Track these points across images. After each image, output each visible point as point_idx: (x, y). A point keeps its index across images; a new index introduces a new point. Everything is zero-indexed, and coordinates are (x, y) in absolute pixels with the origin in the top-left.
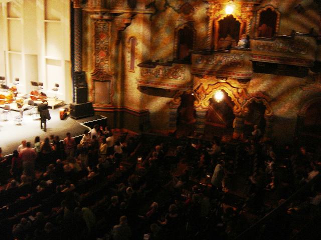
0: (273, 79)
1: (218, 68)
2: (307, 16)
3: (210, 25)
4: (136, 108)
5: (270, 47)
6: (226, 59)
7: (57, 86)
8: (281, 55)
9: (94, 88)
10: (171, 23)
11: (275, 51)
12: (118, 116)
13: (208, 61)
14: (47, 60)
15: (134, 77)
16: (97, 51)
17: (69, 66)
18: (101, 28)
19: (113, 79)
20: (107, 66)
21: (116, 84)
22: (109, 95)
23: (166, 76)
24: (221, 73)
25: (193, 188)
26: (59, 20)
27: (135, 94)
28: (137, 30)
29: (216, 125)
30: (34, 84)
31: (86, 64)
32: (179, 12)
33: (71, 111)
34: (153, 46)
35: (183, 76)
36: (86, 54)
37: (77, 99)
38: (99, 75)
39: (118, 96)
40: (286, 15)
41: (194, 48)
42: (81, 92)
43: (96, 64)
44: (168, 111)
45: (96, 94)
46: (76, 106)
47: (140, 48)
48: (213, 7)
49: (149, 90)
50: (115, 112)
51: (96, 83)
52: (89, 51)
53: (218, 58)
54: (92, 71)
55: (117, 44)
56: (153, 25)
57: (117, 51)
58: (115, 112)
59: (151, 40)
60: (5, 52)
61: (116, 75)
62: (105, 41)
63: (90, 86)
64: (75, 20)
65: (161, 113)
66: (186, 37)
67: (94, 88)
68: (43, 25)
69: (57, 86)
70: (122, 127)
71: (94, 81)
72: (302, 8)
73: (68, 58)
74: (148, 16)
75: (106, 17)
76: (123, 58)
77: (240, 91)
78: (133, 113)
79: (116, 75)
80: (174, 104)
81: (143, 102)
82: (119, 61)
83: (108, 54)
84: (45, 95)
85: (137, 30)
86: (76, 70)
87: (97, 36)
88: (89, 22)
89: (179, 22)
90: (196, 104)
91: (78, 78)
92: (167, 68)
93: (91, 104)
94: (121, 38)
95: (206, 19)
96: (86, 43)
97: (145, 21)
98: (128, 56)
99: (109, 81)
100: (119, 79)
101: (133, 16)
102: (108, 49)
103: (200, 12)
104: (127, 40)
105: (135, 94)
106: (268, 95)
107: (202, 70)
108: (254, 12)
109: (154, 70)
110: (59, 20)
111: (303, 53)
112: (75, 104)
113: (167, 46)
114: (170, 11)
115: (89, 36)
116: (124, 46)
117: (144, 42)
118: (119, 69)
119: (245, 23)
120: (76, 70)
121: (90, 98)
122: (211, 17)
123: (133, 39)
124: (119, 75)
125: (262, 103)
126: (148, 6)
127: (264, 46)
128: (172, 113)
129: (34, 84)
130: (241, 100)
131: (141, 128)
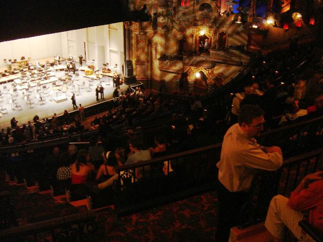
0: (225, 67)
1: (195, 63)
2: (241, 36)
3: (194, 38)
4: (158, 79)
5: (218, 55)
6: (199, 59)
7: (116, 65)
8: (224, 58)
9: (136, 68)
10: (175, 36)
11: (221, 56)
12: (149, 82)
13: (190, 60)
14: (110, 50)
15: (156, 63)
16: (138, 49)
17: (123, 56)
18: (139, 38)
19: (146, 64)
20: (143, 57)
21: (148, 66)
22: (144, 72)
23: (171, 66)
24: (198, 65)
25: (284, 119)
26: (117, 30)
27: (157, 72)
28: (158, 39)
29: (203, 88)
30: (105, 65)
31: (132, 56)
32: (178, 31)
33: (125, 81)
34: (166, 47)
35: (179, 66)
36: (132, 51)
37: (128, 74)
38: (139, 62)
39: (149, 72)
40: (231, 35)
41: (186, 51)
42: (130, 72)
43: (137, 56)
44: (174, 81)
45: (137, 72)
46: (128, 78)
47: (160, 49)
48: (196, 30)
49: (165, 72)
50: (148, 81)
51: (137, 66)
52: (133, 49)
53: (195, 58)
54: (135, 60)
55: (148, 46)
56: (166, 36)
57: (148, 49)
58: (148, 81)
59: (165, 45)
60: (85, 43)
61: (148, 61)
62: (142, 44)
63: (134, 67)
64: (126, 35)
65: (171, 81)
66: (182, 43)
67: (136, 68)
68: (108, 31)
69: (116, 65)
70: (151, 88)
71: (136, 64)
72: (239, 33)
73: (123, 51)
74: (163, 33)
75: (142, 33)
76: (151, 53)
77: (210, 72)
78: (156, 81)
79: (148, 61)
80: (177, 77)
81: (162, 76)
82: (149, 54)
83: (143, 51)
84: (110, 70)
85: (158, 39)
86: (127, 59)
87: (138, 42)
88: (133, 35)
89: (179, 36)
90: (188, 78)
91: (129, 63)
92: (171, 62)
93: (135, 76)
94: (150, 42)
95: (192, 36)
96: (132, 45)
97: (162, 35)
98: (154, 52)
99: (144, 65)
100: (149, 64)
101: (155, 33)
102: (143, 49)
103: (189, 32)
104: (153, 43)
105: (157, 72)
106: (223, 75)
107: (188, 64)
108: (215, 33)
109: (165, 62)
110: (117, 30)
111: (233, 58)
112: (127, 77)
113: (173, 48)
114: (174, 30)
115: (134, 41)
116: (151, 47)
117: (161, 46)
118: (149, 58)
119: (211, 39)
120: (127, 59)
121: (134, 73)
122: (195, 35)
123: (156, 44)
124: (149, 54)
125: (221, 79)
126: (163, 28)
127: (215, 54)
128: (176, 82)
129: (105, 65)
130: (210, 76)
131: (161, 90)
